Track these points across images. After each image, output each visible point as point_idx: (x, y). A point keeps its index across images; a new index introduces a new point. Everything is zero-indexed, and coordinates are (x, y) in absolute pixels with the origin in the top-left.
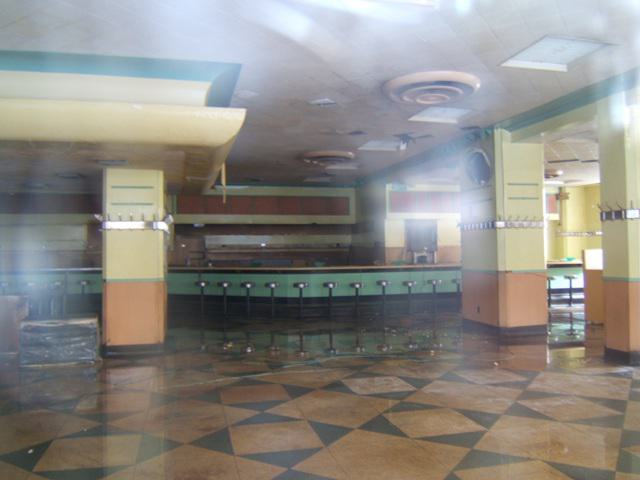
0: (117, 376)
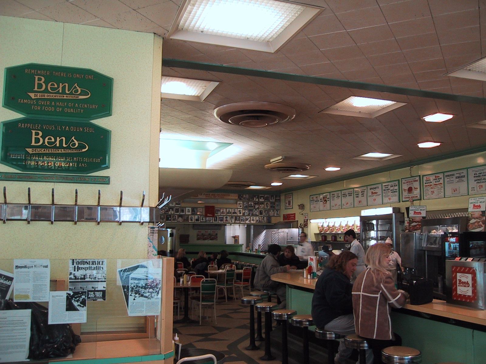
0: (414, 201)
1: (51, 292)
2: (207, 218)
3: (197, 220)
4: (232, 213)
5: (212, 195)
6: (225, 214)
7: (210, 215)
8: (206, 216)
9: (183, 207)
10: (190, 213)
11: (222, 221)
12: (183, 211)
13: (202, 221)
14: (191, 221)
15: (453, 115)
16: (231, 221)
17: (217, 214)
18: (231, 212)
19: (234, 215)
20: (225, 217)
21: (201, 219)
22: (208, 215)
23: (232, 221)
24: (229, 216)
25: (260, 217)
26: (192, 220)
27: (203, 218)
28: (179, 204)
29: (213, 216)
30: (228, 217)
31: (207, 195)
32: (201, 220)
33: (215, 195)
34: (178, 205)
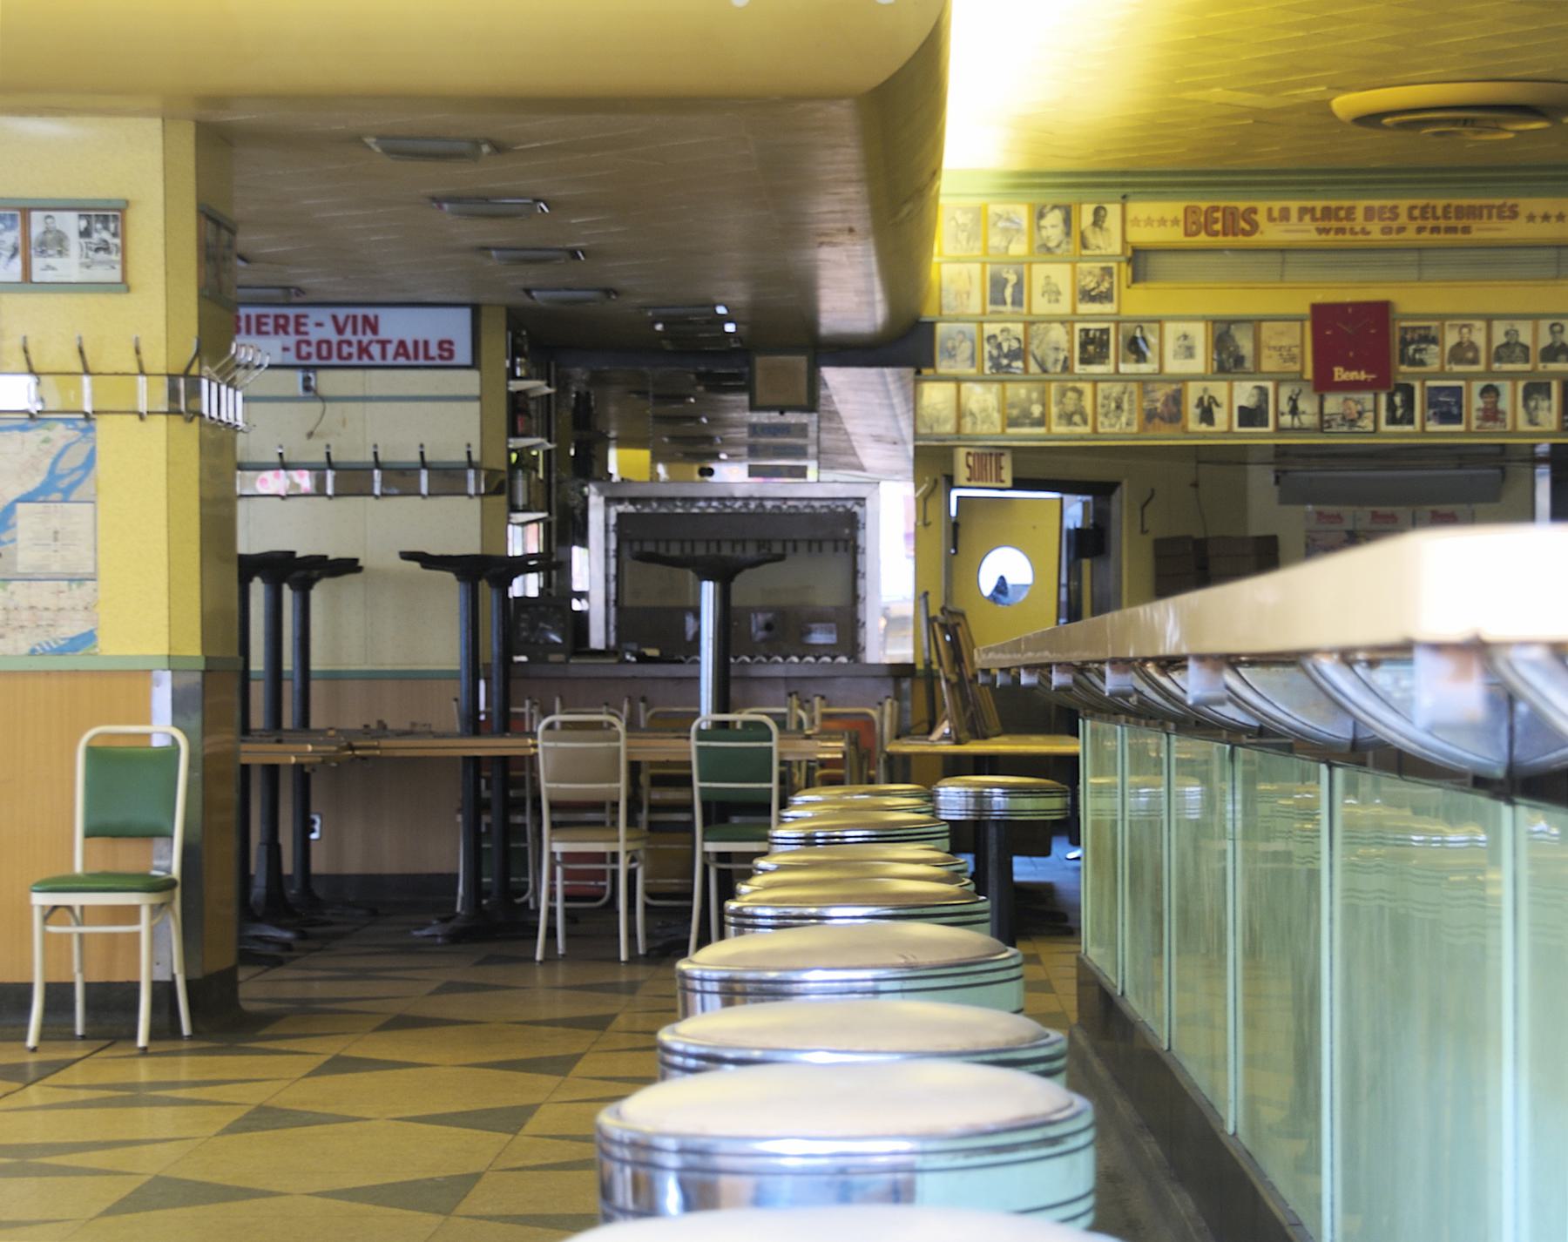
1: (503, 312)
2: (1333, 403)
3: (1250, 416)
4: (1534, 354)
5: (1369, 213)
6: (1480, 368)
7: (1353, 375)
8: (1323, 384)
9: (1140, 322)
10: (1198, 364)
11: (1457, 419)
12: (1135, 348)
13: (1286, 420)
14: (1204, 427)
15: (728, 310)
16: (1532, 422)
17: (1413, 362)
18: (1525, 348)
19: (1553, 367)
20: (1477, 386)
21: (1285, 406)
22: (1340, 374)
23: (1542, 416)
24: (1513, 376)
25: (1270, 385)
26: (1207, 416)
27: (1293, 401)
28: (1105, 297)
29: (1382, 381)
30: (1505, 387)
31: (1328, 213)
32: (1278, 414)
33: (1396, 217)
34: (1093, 299)
